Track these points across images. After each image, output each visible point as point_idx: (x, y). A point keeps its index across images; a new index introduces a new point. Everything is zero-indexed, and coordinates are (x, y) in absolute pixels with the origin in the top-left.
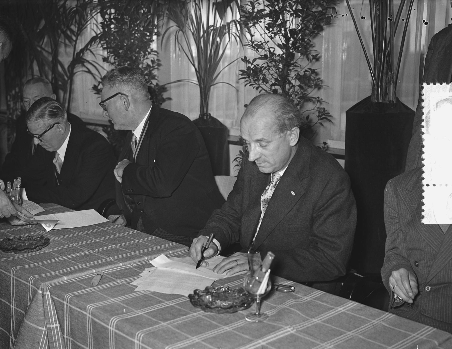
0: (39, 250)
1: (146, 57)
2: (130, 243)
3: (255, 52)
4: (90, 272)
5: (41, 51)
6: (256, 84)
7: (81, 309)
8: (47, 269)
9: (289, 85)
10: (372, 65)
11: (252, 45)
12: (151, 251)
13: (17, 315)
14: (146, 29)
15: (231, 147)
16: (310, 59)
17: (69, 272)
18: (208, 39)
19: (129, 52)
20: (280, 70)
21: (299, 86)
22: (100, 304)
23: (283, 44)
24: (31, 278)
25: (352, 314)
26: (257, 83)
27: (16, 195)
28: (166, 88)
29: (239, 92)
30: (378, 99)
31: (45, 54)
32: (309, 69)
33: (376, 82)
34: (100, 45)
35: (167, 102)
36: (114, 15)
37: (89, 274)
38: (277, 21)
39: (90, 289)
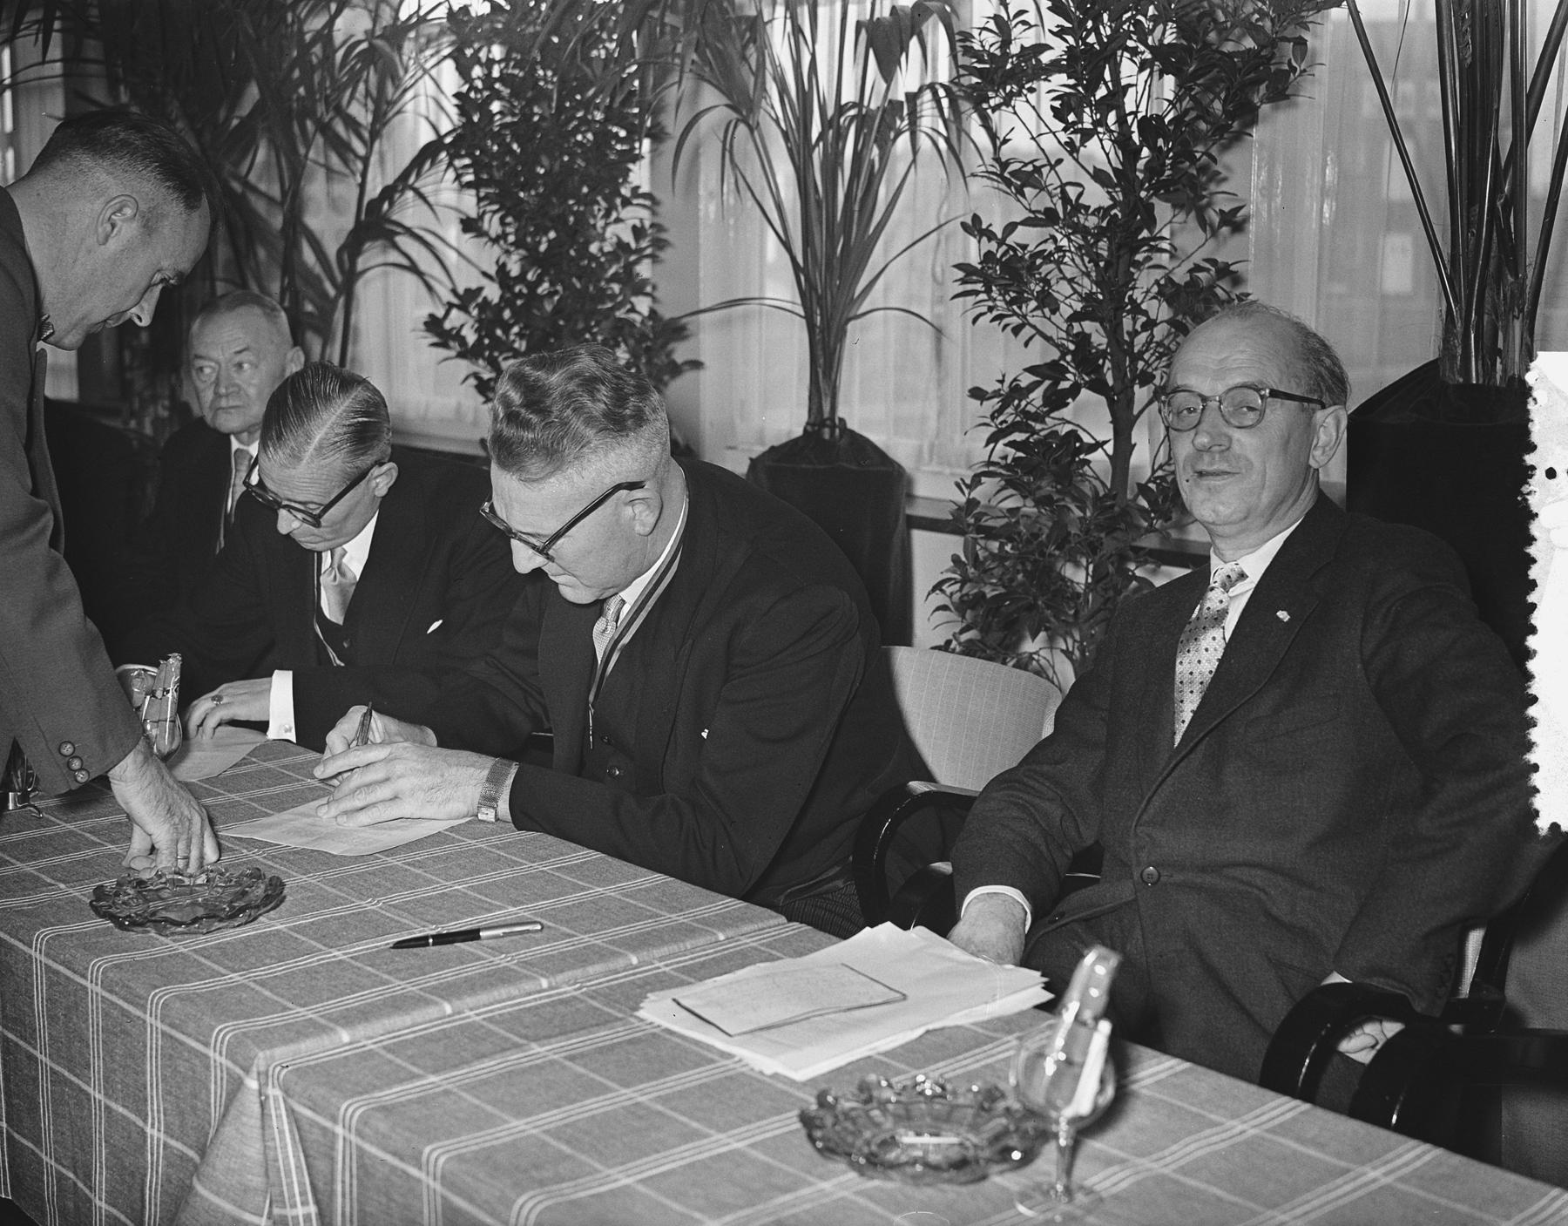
0: (246, 923)
1: (614, 215)
2: (572, 898)
3: (1012, 199)
4: (432, 1012)
5: (243, 196)
6: (1015, 314)
7: (402, 1159)
8: (275, 998)
9: (1135, 320)
10: (1446, 250)
11: (1001, 176)
12: (648, 933)
13: (169, 1165)
14: (613, 116)
15: (919, 538)
16: (1211, 226)
17: (356, 1008)
18: (840, 154)
19: (554, 200)
20: (1102, 264)
21: (1170, 322)
22: (471, 1142)
23: (1115, 170)
24: (218, 1034)
25: (1421, 1193)
26: (1017, 310)
27: (162, 718)
28: (683, 328)
29: (945, 341)
30: (1466, 370)
31: (260, 206)
32: (1207, 260)
33: (1460, 309)
34: (451, 174)
35: (688, 376)
36: (503, 65)
37: (430, 1021)
38: (1092, 89)
39: (433, 1078)
